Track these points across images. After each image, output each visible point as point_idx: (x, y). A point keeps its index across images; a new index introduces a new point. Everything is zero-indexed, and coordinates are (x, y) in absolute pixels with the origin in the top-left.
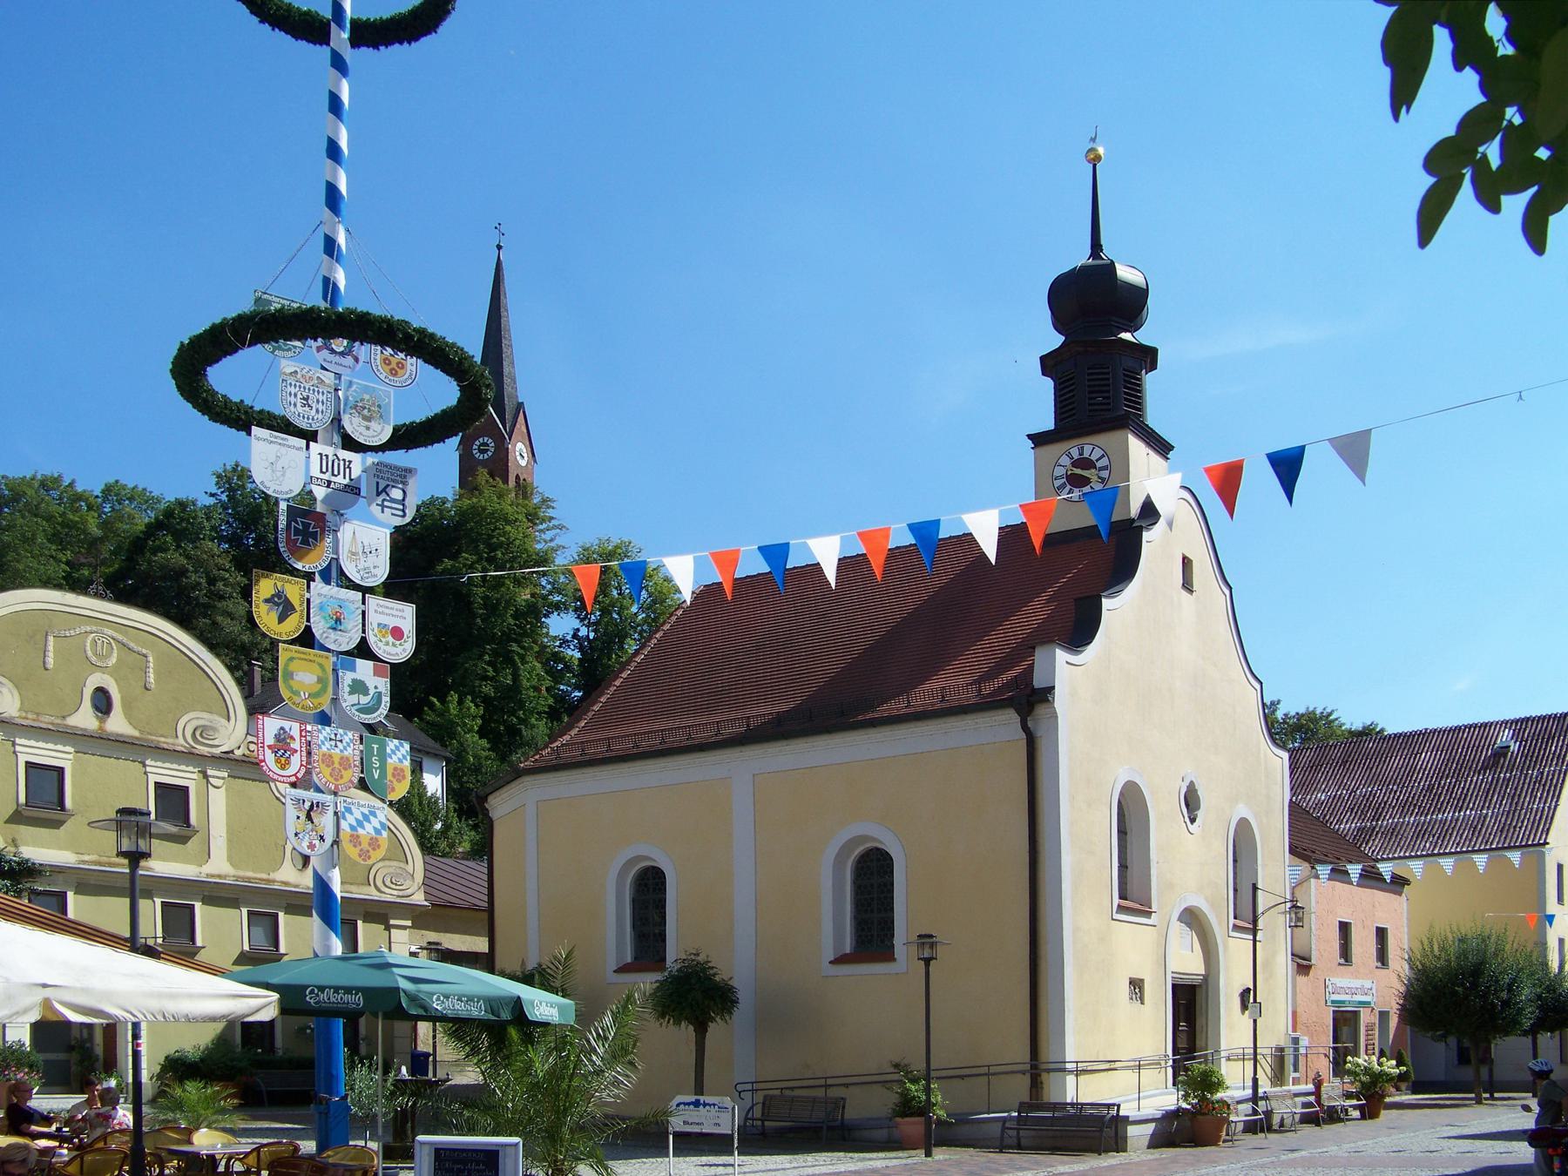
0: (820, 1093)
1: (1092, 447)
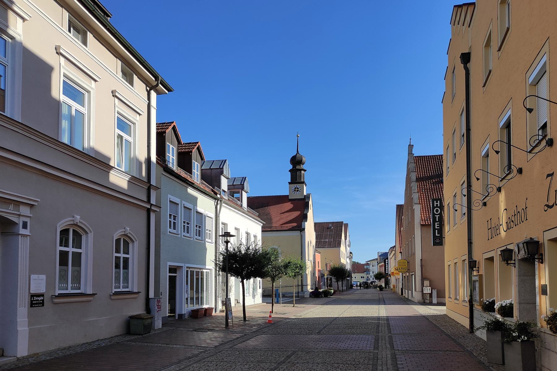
1: (298, 186)
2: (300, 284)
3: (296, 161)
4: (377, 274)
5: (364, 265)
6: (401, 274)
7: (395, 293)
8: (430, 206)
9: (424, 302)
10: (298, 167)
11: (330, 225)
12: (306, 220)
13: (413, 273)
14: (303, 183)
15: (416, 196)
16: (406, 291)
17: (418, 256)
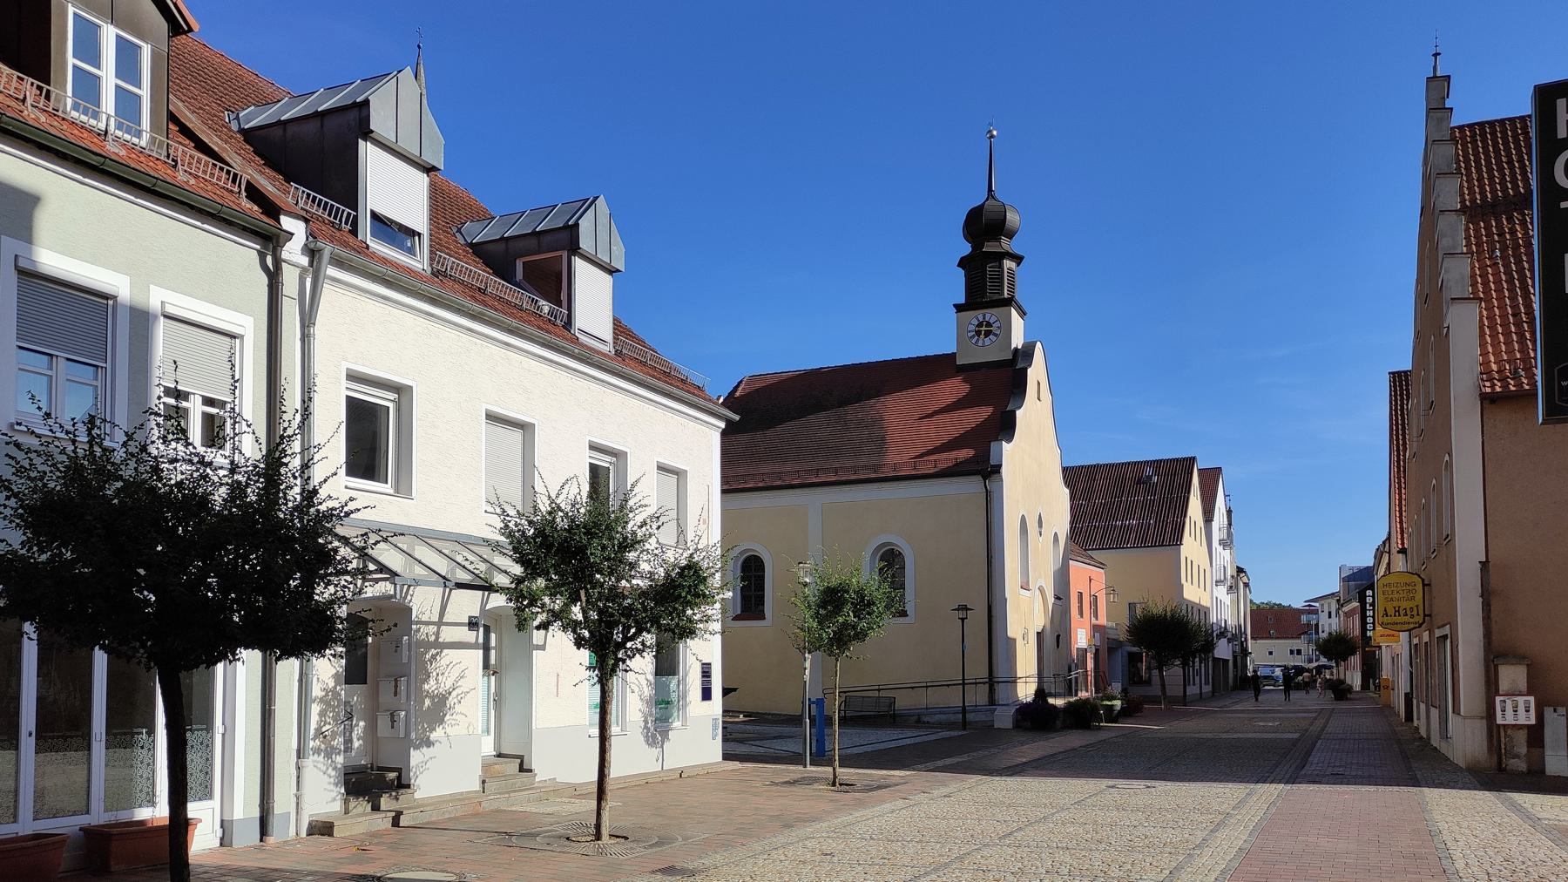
0: (876, 694)
1: (991, 315)
2: (978, 671)
3: (985, 227)
4: (1327, 641)
5: (1299, 612)
6: (1404, 636)
7: (1389, 708)
8: (1530, 312)
9: (1501, 769)
10: (989, 247)
11: (1149, 471)
12: (1010, 438)
13: (1446, 630)
14: (1009, 302)
15: (1458, 273)
16: (1423, 706)
17: (1469, 547)
